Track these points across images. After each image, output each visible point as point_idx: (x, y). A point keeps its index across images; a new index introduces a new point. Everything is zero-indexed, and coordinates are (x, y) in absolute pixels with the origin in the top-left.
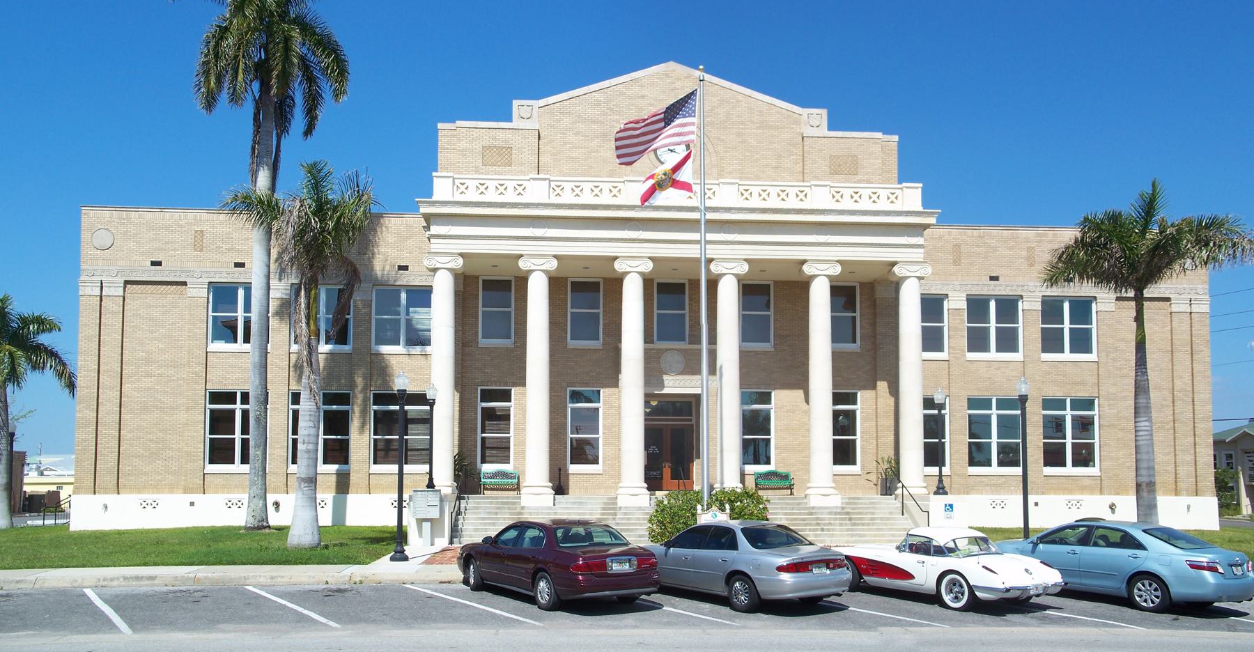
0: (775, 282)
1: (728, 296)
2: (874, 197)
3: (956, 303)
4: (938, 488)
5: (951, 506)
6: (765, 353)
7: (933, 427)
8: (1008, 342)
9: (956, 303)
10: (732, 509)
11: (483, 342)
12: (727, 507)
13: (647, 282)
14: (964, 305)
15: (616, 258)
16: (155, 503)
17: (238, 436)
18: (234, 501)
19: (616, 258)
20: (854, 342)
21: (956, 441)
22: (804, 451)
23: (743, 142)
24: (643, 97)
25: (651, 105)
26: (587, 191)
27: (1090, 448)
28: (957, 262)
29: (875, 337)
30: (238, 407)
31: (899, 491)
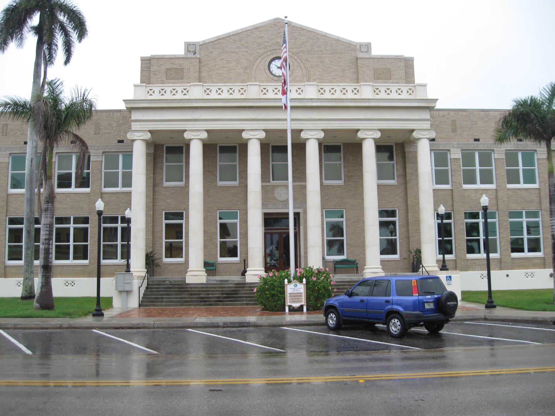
0: (344, 144)
1: (369, 151)
2: (355, 91)
3: (456, 154)
4: (443, 266)
5: (450, 277)
6: (339, 186)
7: (444, 230)
8: (487, 178)
9: (456, 154)
10: (307, 283)
11: (166, 184)
12: (304, 280)
13: (321, 145)
14: (459, 156)
15: (302, 130)
16: (532, 275)
17: (119, 242)
18: (70, 282)
19: (243, 130)
20: (394, 179)
21: (459, 238)
22: (362, 246)
23: (322, 62)
24: (261, 37)
25: (266, 42)
26: (350, 91)
27: (537, 241)
28: (454, 131)
29: (406, 176)
30: (119, 226)
31: (421, 270)
